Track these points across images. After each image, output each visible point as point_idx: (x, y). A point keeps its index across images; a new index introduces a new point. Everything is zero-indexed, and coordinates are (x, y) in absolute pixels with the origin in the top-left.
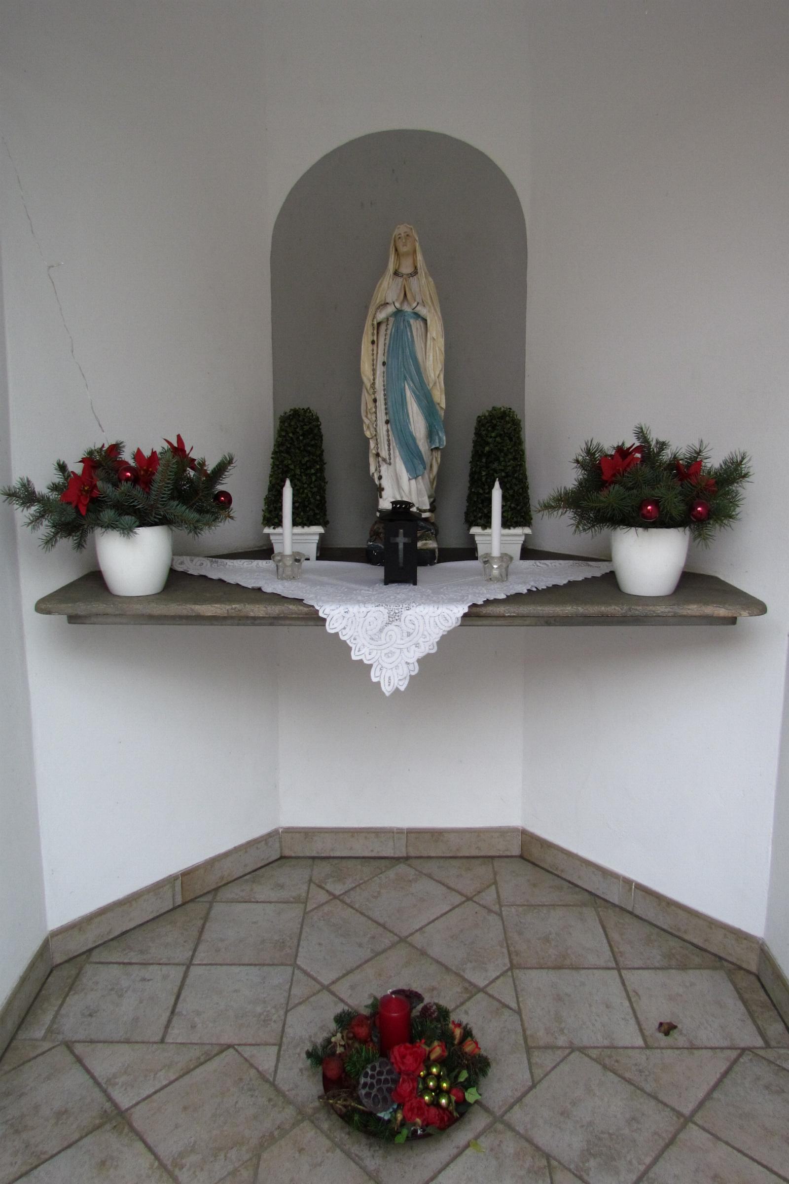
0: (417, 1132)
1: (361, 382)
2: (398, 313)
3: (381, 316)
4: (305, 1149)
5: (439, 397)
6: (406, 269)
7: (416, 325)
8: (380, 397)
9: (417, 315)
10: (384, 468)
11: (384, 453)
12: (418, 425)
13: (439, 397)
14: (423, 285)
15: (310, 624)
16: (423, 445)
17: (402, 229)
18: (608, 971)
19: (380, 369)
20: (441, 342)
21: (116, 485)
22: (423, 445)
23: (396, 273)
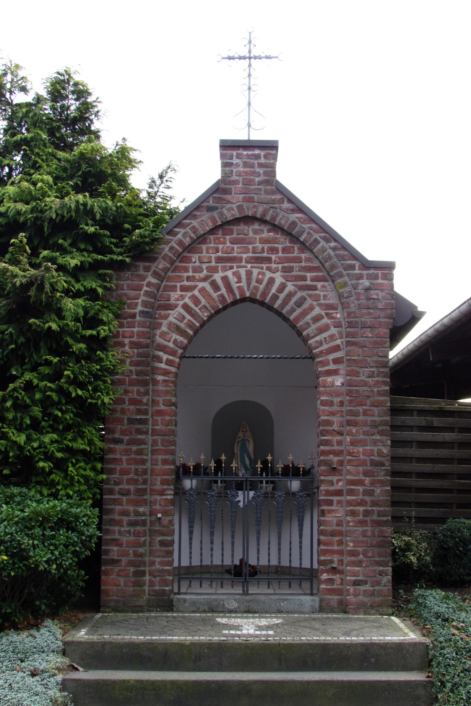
0: (71, 394)
1: (234, 454)
2: (243, 439)
3: (239, 440)
4: (27, 91)
5: (252, 456)
6: (245, 430)
7: (247, 442)
8: (239, 456)
9: (247, 440)
10: (240, 472)
11: (240, 468)
12: (247, 462)
13: (252, 456)
14: (248, 433)
15: (465, 305)
16: (249, 467)
17: (243, 423)
18: (224, 548)
19: (239, 451)
20: (253, 445)
21: (114, 342)
22: (249, 467)
23: (243, 431)
